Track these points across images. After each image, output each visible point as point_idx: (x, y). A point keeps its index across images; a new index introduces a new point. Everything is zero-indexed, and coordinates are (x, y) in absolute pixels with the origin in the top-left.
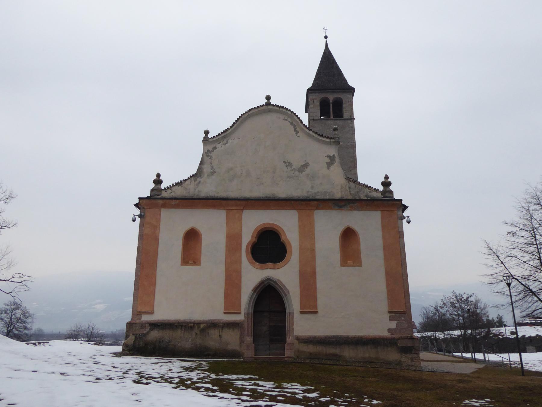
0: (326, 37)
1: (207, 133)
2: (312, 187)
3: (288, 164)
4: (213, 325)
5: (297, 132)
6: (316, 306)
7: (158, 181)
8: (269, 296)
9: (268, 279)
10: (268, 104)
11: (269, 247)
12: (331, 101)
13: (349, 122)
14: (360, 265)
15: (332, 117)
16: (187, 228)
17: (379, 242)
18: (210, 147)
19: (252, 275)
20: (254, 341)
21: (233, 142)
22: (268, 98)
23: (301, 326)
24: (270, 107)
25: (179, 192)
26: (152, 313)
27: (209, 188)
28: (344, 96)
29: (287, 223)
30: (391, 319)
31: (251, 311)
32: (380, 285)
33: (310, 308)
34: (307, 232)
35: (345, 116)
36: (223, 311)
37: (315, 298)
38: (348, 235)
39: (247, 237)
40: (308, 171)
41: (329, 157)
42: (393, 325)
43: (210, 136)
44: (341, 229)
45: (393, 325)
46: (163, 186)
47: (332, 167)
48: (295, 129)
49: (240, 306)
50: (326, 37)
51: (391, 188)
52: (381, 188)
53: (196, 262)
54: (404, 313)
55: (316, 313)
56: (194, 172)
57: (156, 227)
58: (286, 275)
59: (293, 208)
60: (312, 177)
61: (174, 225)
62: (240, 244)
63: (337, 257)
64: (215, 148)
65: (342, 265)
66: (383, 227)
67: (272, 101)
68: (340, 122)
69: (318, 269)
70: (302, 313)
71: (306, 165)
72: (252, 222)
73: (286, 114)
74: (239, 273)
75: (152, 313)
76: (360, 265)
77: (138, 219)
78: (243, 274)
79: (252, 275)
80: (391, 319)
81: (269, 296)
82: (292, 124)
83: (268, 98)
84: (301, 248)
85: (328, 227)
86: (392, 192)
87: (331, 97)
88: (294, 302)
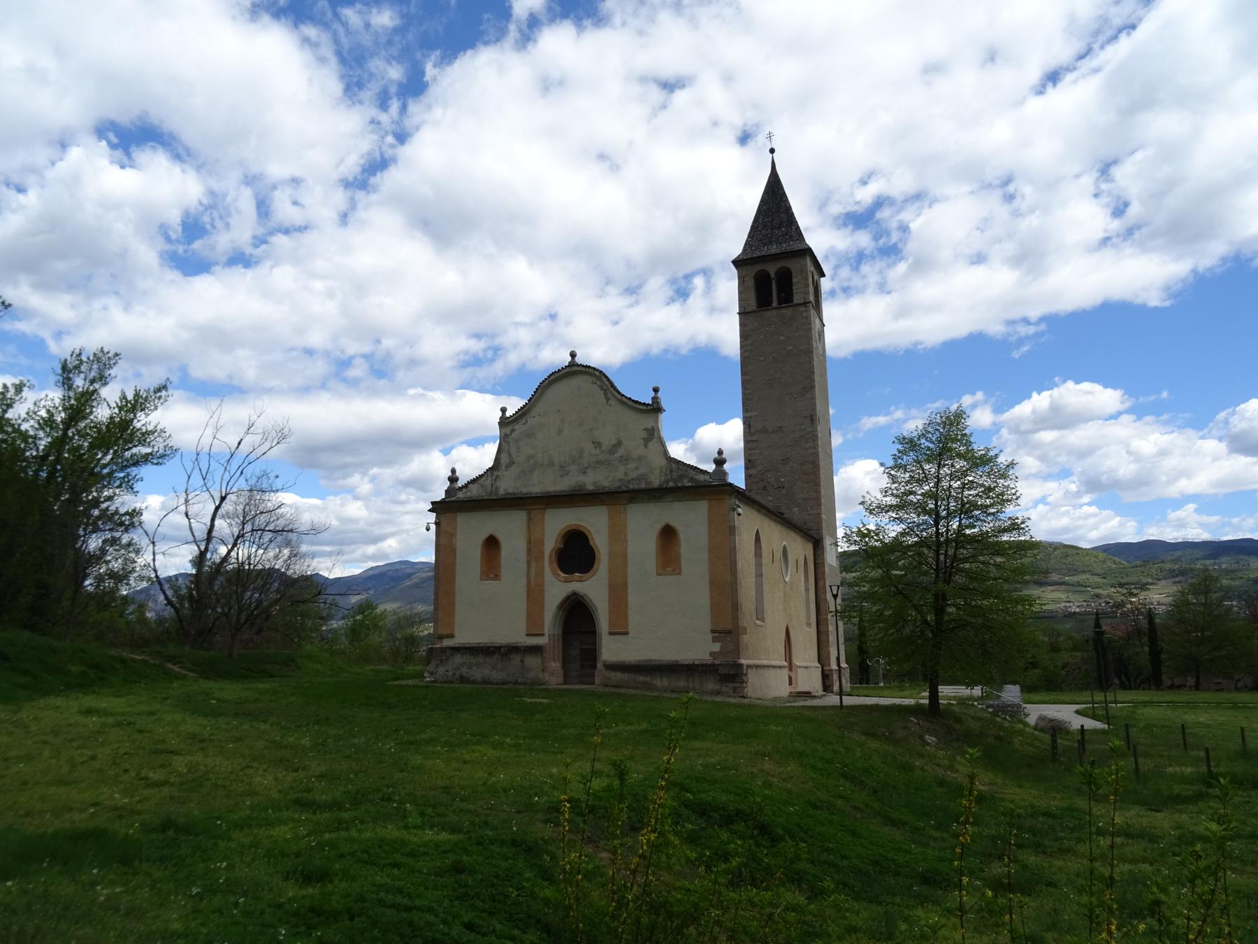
0: (772, 151)
1: (504, 410)
2: (626, 474)
3: (597, 444)
4: (513, 649)
5: (608, 399)
6: (626, 626)
7: (453, 479)
8: (577, 614)
9: (575, 594)
10: (573, 364)
11: (576, 554)
12: (773, 276)
13: (802, 309)
14: (680, 574)
15: (775, 304)
16: (486, 535)
17: (704, 541)
18: (508, 430)
19: (557, 589)
20: (564, 667)
21: (532, 421)
22: (573, 355)
23: (611, 649)
24: (575, 368)
25: (475, 491)
26: (451, 636)
27: (507, 485)
28: (793, 265)
29: (595, 522)
30: (714, 640)
31: (558, 631)
32: (702, 598)
33: (619, 630)
34: (618, 534)
35: (797, 299)
36: (525, 632)
37: (625, 617)
38: (668, 534)
39: (551, 542)
40: (621, 452)
41: (646, 429)
42: (716, 647)
43: (508, 414)
44: (659, 527)
45: (716, 647)
46: (460, 484)
47: (650, 444)
48: (606, 394)
49: (543, 626)
50: (772, 151)
51: (726, 466)
52: (710, 467)
53: (497, 577)
54: (730, 632)
55: (626, 633)
56: (491, 465)
57: (452, 536)
58: (594, 588)
59: (603, 503)
60: (625, 460)
61: (473, 529)
62: (543, 552)
63: (651, 564)
64: (513, 430)
65: (658, 574)
66: (711, 522)
67: (579, 360)
68: (787, 312)
69: (630, 580)
70: (611, 634)
71: (619, 444)
72: (556, 523)
73: (593, 375)
74: (541, 587)
75: (451, 636)
76: (680, 574)
77: (433, 527)
78: (546, 588)
79: (557, 589)
80: (714, 640)
81: (577, 614)
82: (601, 388)
83: (573, 355)
84: (610, 554)
85: (643, 523)
86: (725, 474)
87: (772, 269)
88: (603, 622)
